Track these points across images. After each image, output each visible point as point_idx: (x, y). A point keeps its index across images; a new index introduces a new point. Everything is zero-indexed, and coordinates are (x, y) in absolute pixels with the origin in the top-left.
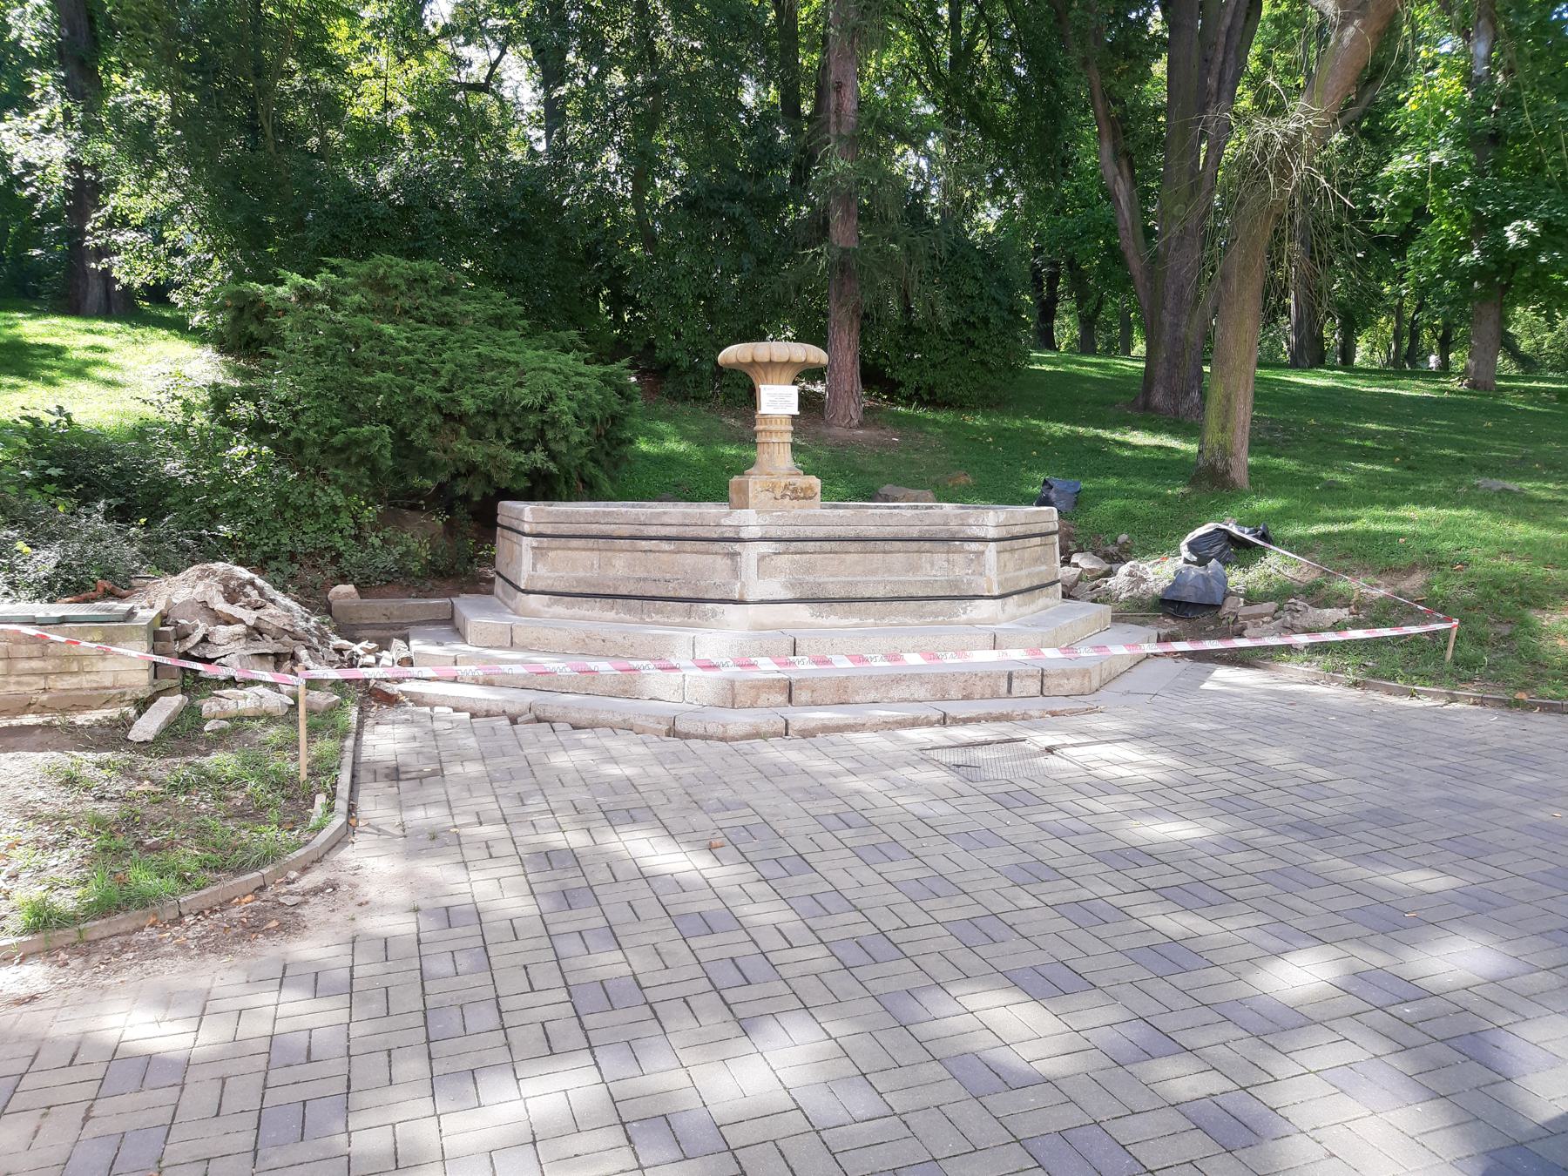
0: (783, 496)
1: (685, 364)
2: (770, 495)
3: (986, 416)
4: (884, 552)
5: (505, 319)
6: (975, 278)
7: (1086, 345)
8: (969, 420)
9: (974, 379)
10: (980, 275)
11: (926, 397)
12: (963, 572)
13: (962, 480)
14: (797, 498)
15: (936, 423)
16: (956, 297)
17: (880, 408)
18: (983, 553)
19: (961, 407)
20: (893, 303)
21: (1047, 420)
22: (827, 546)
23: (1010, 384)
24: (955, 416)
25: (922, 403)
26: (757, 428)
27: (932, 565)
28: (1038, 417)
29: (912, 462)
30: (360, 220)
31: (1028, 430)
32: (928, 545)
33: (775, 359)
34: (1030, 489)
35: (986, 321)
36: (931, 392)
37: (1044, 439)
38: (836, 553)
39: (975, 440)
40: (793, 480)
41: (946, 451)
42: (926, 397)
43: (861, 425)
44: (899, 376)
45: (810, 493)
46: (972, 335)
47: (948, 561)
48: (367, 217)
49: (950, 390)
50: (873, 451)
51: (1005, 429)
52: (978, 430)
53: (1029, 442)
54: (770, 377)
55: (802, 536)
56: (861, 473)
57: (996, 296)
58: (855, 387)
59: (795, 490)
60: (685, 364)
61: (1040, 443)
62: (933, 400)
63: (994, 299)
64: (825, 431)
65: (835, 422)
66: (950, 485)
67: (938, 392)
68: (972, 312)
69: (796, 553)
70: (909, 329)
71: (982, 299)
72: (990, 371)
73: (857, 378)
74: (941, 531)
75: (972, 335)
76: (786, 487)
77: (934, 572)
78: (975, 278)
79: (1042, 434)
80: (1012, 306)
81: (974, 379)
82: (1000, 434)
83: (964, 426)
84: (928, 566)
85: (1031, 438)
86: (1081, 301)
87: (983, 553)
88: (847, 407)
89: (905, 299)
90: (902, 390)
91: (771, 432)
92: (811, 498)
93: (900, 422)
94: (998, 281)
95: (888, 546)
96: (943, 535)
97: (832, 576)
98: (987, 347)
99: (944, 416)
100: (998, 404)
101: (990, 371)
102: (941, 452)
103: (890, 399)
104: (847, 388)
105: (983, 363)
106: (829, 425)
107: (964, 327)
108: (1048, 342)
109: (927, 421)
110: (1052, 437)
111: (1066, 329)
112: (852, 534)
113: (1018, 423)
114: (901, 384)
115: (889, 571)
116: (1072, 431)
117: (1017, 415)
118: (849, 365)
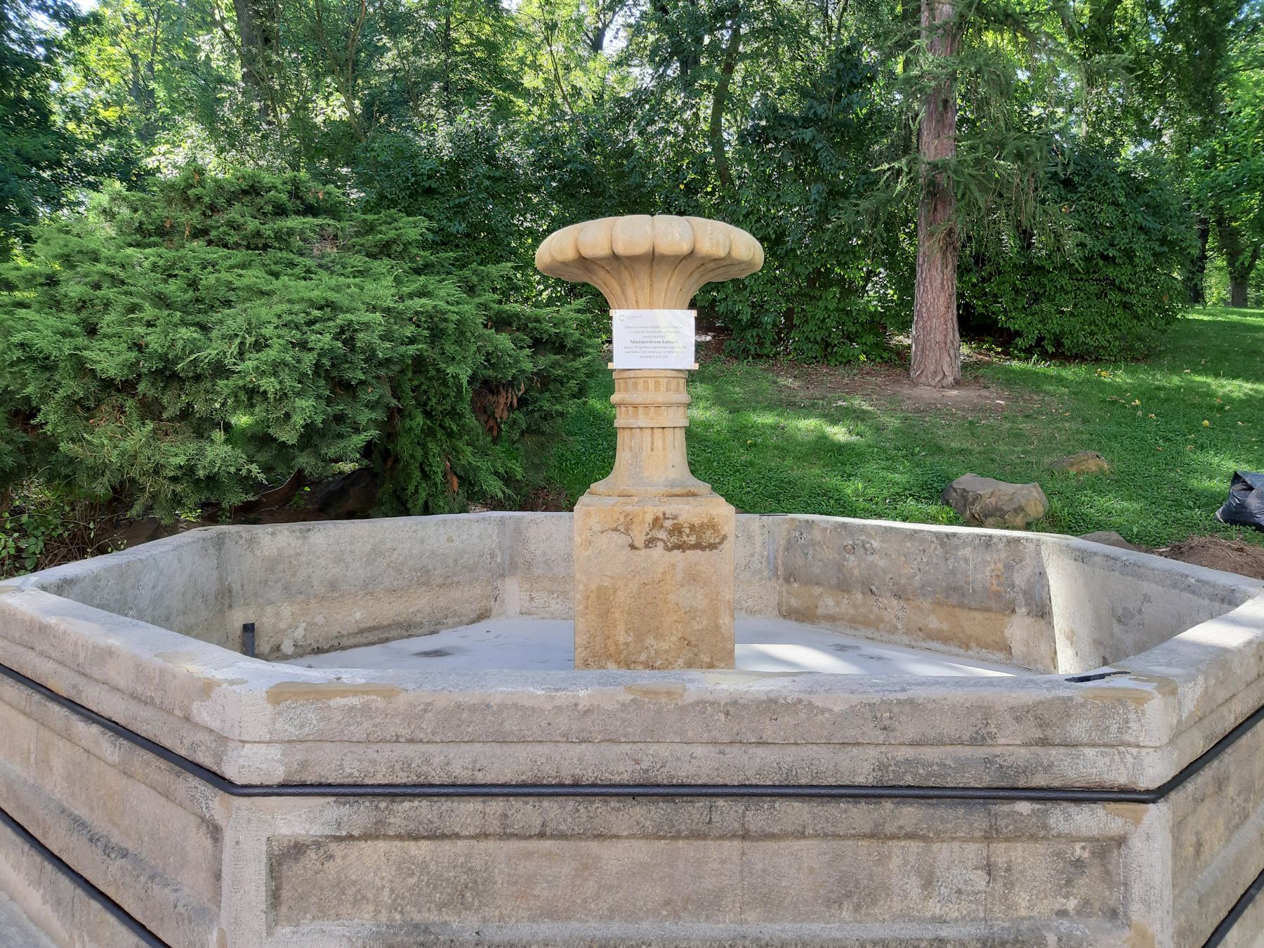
0: (650, 543)
1: (745, 318)
2: (623, 540)
3: (1133, 373)
4: (745, 836)
5: (395, 247)
6: (1115, 204)
7: (1239, 299)
8: (1106, 376)
9: (1113, 326)
10: (1122, 199)
11: (1051, 349)
12: (1045, 907)
13: (1092, 465)
14: (681, 547)
15: (1060, 380)
16: (1091, 226)
17: (989, 364)
18: (1121, 841)
19: (1097, 360)
20: (1009, 241)
21: (1217, 375)
22: (526, 812)
23: (1164, 332)
24: (1088, 371)
25: (1045, 356)
26: (615, 398)
27: (928, 882)
28: (1205, 371)
29: (1018, 436)
30: (408, 179)
31: (1192, 389)
32: (910, 814)
33: (621, 250)
34: (1207, 484)
35: (1129, 254)
36: (1058, 343)
37: (1217, 402)
38: (562, 836)
39: (1114, 402)
40: (674, 507)
41: (1073, 418)
42: (1051, 349)
43: (957, 384)
44: (1016, 326)
45: (709, 536)
46: (1111, 272)
47: (989, 869)
48: (414, 175)
49: (1082, 339)
50: (964, 418)
51: (1159, 388)
52: (1120, 390)
53: (1194, 406)
54: (630, 292)
55: (437, 776)
56: (939, 450)
57: (1144, 223)
58: (950, 337)
59: (677, 530)
60: (745, 318)
61: (1211, 408)
62: (1059, 351)
63: (1141, 228)
64: (906, 391)
65: (923, 379)
66: (1073, 472)
67: (1067, 342)
68: (1112, 245)
69: (416, 837)
70: (1031, 269)
71: (1125, 229)
72: (1137, 317)
73: (953, 324)
74: (963, 765)
75: (1111, 272)
76: (657, 523)
77: (934, 908)
78: (1115, 204)
79: (1212, 395)
80: (1165, 237)
81: (1113, 326)
82: (1150, 395)
83: (1100, 385)
84: (914, 885)
85: (1197, 400)
86: (1232, 257)
87: (1121, 841)
88: (939, 362)
89: (1025, 236)
90: (1019, 341)
91: (635, 406)
92: (712, 547)
93: (1010, 380)
94: (1147, 206)
95: (758, 816)
96: (971, 778)
97: (551, 913)
98: (1132, 286)
99: (1072, 372)
100: (1146, 357)
101: (1137, 317)
102: (1064, 420)
103: (1006, 353)
104: (939, 338)
105: (1126, 306)
106: (915, 384)
107: (1101, 263)
108: (1197, 296)
109: (1047, 377)
110: (1228, 399)
111: (1216, 285)
112: (623, 772)
113: (1176, 380)
114: (1018, 334)
115: (767, 901)
116: (1256, 391)
117: (1174, 370)
118: (943, 309)
